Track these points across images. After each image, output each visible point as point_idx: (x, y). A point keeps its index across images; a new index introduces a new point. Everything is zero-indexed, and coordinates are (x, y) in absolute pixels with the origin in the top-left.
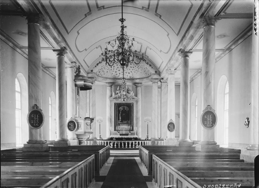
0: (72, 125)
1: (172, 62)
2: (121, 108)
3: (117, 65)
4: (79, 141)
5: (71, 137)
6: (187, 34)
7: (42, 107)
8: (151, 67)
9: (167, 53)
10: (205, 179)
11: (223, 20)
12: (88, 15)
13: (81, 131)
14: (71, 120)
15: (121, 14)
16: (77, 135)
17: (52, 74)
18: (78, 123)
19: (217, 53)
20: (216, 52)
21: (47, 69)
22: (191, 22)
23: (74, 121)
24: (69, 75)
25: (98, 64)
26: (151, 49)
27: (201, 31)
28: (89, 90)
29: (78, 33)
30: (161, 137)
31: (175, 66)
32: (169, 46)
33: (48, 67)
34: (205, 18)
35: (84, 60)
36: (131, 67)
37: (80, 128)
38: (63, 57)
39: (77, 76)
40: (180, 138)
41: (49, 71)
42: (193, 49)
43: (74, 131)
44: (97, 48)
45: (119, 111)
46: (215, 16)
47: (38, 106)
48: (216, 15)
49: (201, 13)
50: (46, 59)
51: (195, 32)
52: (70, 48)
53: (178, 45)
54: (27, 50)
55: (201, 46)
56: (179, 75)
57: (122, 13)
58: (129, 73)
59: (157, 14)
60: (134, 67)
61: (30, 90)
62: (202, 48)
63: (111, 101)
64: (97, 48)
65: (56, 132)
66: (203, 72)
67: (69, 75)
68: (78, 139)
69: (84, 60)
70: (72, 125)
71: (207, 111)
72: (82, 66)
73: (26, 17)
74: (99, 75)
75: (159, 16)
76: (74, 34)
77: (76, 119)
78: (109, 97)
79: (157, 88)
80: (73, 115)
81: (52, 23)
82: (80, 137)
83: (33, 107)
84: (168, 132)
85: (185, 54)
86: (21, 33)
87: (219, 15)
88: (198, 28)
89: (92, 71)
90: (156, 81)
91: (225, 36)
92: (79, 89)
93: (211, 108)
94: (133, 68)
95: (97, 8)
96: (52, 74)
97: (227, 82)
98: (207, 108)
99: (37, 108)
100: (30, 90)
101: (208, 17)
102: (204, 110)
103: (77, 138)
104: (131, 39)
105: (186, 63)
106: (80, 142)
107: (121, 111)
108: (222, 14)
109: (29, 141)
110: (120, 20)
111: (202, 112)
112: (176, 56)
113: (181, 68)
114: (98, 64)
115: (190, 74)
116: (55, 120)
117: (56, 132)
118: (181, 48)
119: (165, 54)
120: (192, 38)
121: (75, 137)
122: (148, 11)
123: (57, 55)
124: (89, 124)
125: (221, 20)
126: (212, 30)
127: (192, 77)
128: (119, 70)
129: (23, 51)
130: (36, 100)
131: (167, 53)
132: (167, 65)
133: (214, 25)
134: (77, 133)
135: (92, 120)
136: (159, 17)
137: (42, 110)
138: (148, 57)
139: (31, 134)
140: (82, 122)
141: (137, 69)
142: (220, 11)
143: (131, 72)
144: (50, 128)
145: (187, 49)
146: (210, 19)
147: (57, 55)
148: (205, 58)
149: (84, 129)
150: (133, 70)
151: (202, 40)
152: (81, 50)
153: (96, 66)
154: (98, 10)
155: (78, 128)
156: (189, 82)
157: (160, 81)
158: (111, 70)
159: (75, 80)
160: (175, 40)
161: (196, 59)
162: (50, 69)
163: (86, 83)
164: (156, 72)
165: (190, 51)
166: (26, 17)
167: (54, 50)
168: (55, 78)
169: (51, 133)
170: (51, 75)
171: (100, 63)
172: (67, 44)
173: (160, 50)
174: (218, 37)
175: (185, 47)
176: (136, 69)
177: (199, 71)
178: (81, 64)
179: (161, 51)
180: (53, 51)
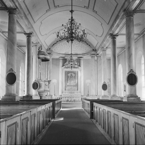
0: (36, 86)
1: (104, 43)
2: (69, 75)
3: (67, 45)
4: (40, 97)
5: (34, 93)
6: (114, 23)
7: (15, 70)
8: (90, 47)
9: (101, 36)
10: (131, 112)
11: (138, 13)
12: (48, 11)
13: (42, 89)
14: (35, 82)
15: (73, 5)
16: (39, 93)
17: (22, 51)
18: (39, 84)
19: (135, 36)
20: (135, 36)
21: (19, 47)
22: (117, 15)
23: (37, 82)
24: (34, 51)
25: (54, 45)
26: (90, 34)
27: (124, 20)
28: (47, 62)
29: (42, 23)
30: (97, 94)
31: (107, 45)
32: (102, 32)
33: (21, 46)
34: (127, 12)
35: (45, 42)
36: (76, 47)
37: (41, 87)
38: (30, 38)
39: (40, 53)
40: (112, 94)
41: (21, 49)
42: (119, 33)
43: (37, 90)
44: (53, 33)
45: (68, 77)
46: (133, 11)
47: (13, 69)
48: (133, 10)
49: (123, 9)
50: (19, 40)
51: (120, 22)
52: (36, 33)
53: (109, 31)
54: (7, 34)
55: (124, 31)
56: (109, 52)
57: (72, 5)
58: (75, 51)
59: (94, 11)
60: (78, 47)
61: (8, 58)
62: (125, 33)
63: (62, 70)
64: (53, 33)
65: (24, 90)
66: (127, 47)
67: (34, 51)
68: (40, 95)
69: (45, 42)
70: (36, 86)
71: (130, 73)
72: (43, 45)
73: (7, 11)
74: (55, 52)
75: (95, 12)
76: (38, 23)
77: (39, 81)
78: (61, 67)
79: (94, 61)
80: (36, 79)
81: (24, 15)
82: (41, 94)
83: (10, 71)
84: (103, 91)
85: (113, 37)
86: (3, 22)
87: (136, 10)
88: (122, 19)
89: (50, 49)
90: (94, 56)
91: (140, 25)
92: (41, 61)
93: (133, 72)
94: (77, 47)
95: (55, 7)
96: (22, 51)
97: (142, 55)
98: (130, 72)
99: (12, 71)
100: (8, 58)
101: (129, 11)
102: (128, 73)
103: (39, 94)
104: (78, 24)
105: (114, 43)
106: (41, 97)
107: (69, 76)
108: (138, 9)
109: (6, 94)
110: (70, 11)
111: (127, 75)
112: (107, 38)
113: (111, 46)
114: (54, 45)
115: (117, 51)
116: (24, 82)
117: (24, 90)
118: (111, 32)
119: (99, 37)
120: (118, 26)
121: (37, 93)
122: (88, 9)
123: (27, 37)
124: (47, 85)
125: (137, 14)
126: (132, 19)
127: (118, 53)
128: (68, 49)
129: (4, 35)
130: (12, 65)
131: (101, 36)
132: (101, 45)
133: (133, 16)
134: (38, 91)
135: (49, 82)
136: (95, 13)
137: (15, 73)
138: (88, 40)
139: (7, 89)
140: (43, 84)
141: (80, 48)
142: (136, 8)
143: (77, 50)
144: (20, 88)
145: (115, 33)
146: (130, 12)
147: (27, 37)
148: (128, 37)
149: (44, 88)
150: (77, 48)
151: (125, 27)
152: (42, 34)
153: (52, 46)
154: (55, 8)
155: (40, 88)
156: (117, 56)
157: (96, 56)
158: (63, 48)
159: (38, 54)
160: (106, 28)
161: (121, 40)
162: (22, 47)
163: (46, 57)
164: (93, 50)
165: (117, 35)
166: (7, 11)
167: (25, 34)
168: (25, 53)
169: (21, 90)
170: (22, 52)
171: (55, 43)
172: (34, 30)
173: (96, 35)
174: (135, 25)
175: (113, 32)
176: (79, 48)
177: (123, 48)
178: (42, 44)
179: (97, 35)
180: (24, 34)
